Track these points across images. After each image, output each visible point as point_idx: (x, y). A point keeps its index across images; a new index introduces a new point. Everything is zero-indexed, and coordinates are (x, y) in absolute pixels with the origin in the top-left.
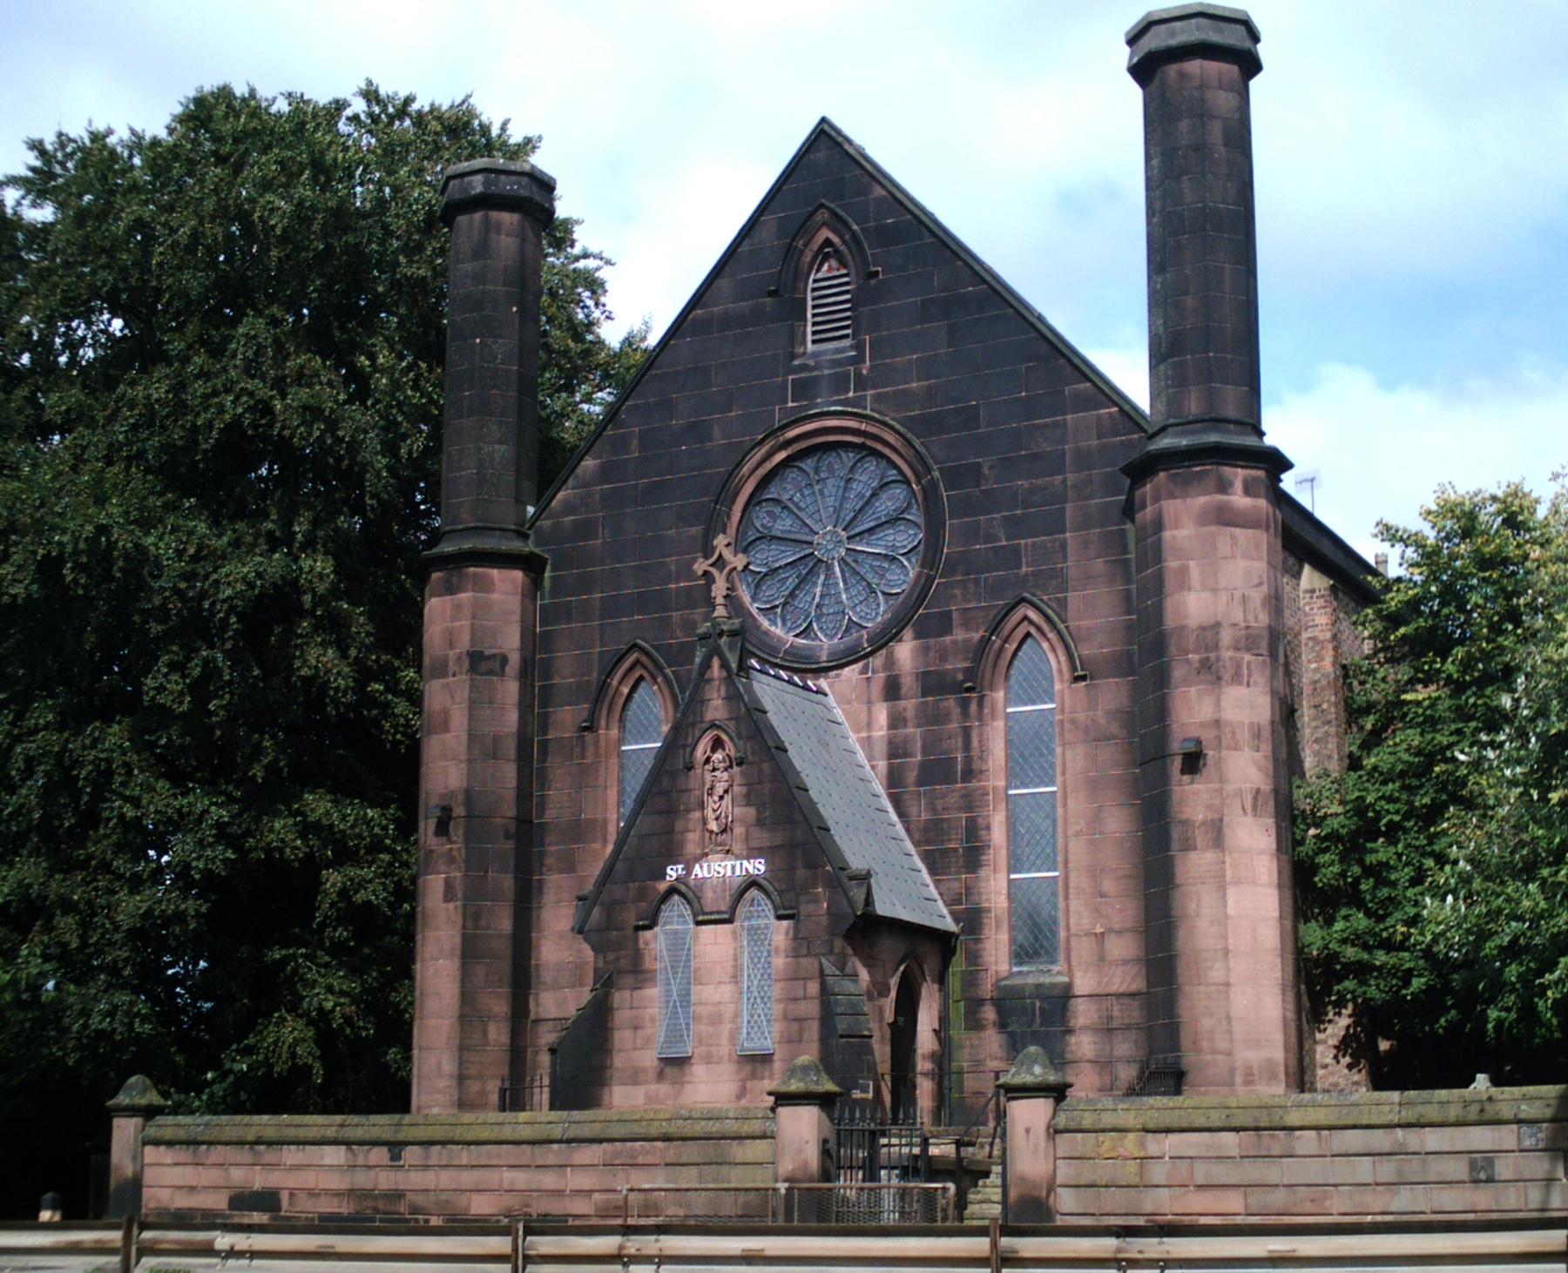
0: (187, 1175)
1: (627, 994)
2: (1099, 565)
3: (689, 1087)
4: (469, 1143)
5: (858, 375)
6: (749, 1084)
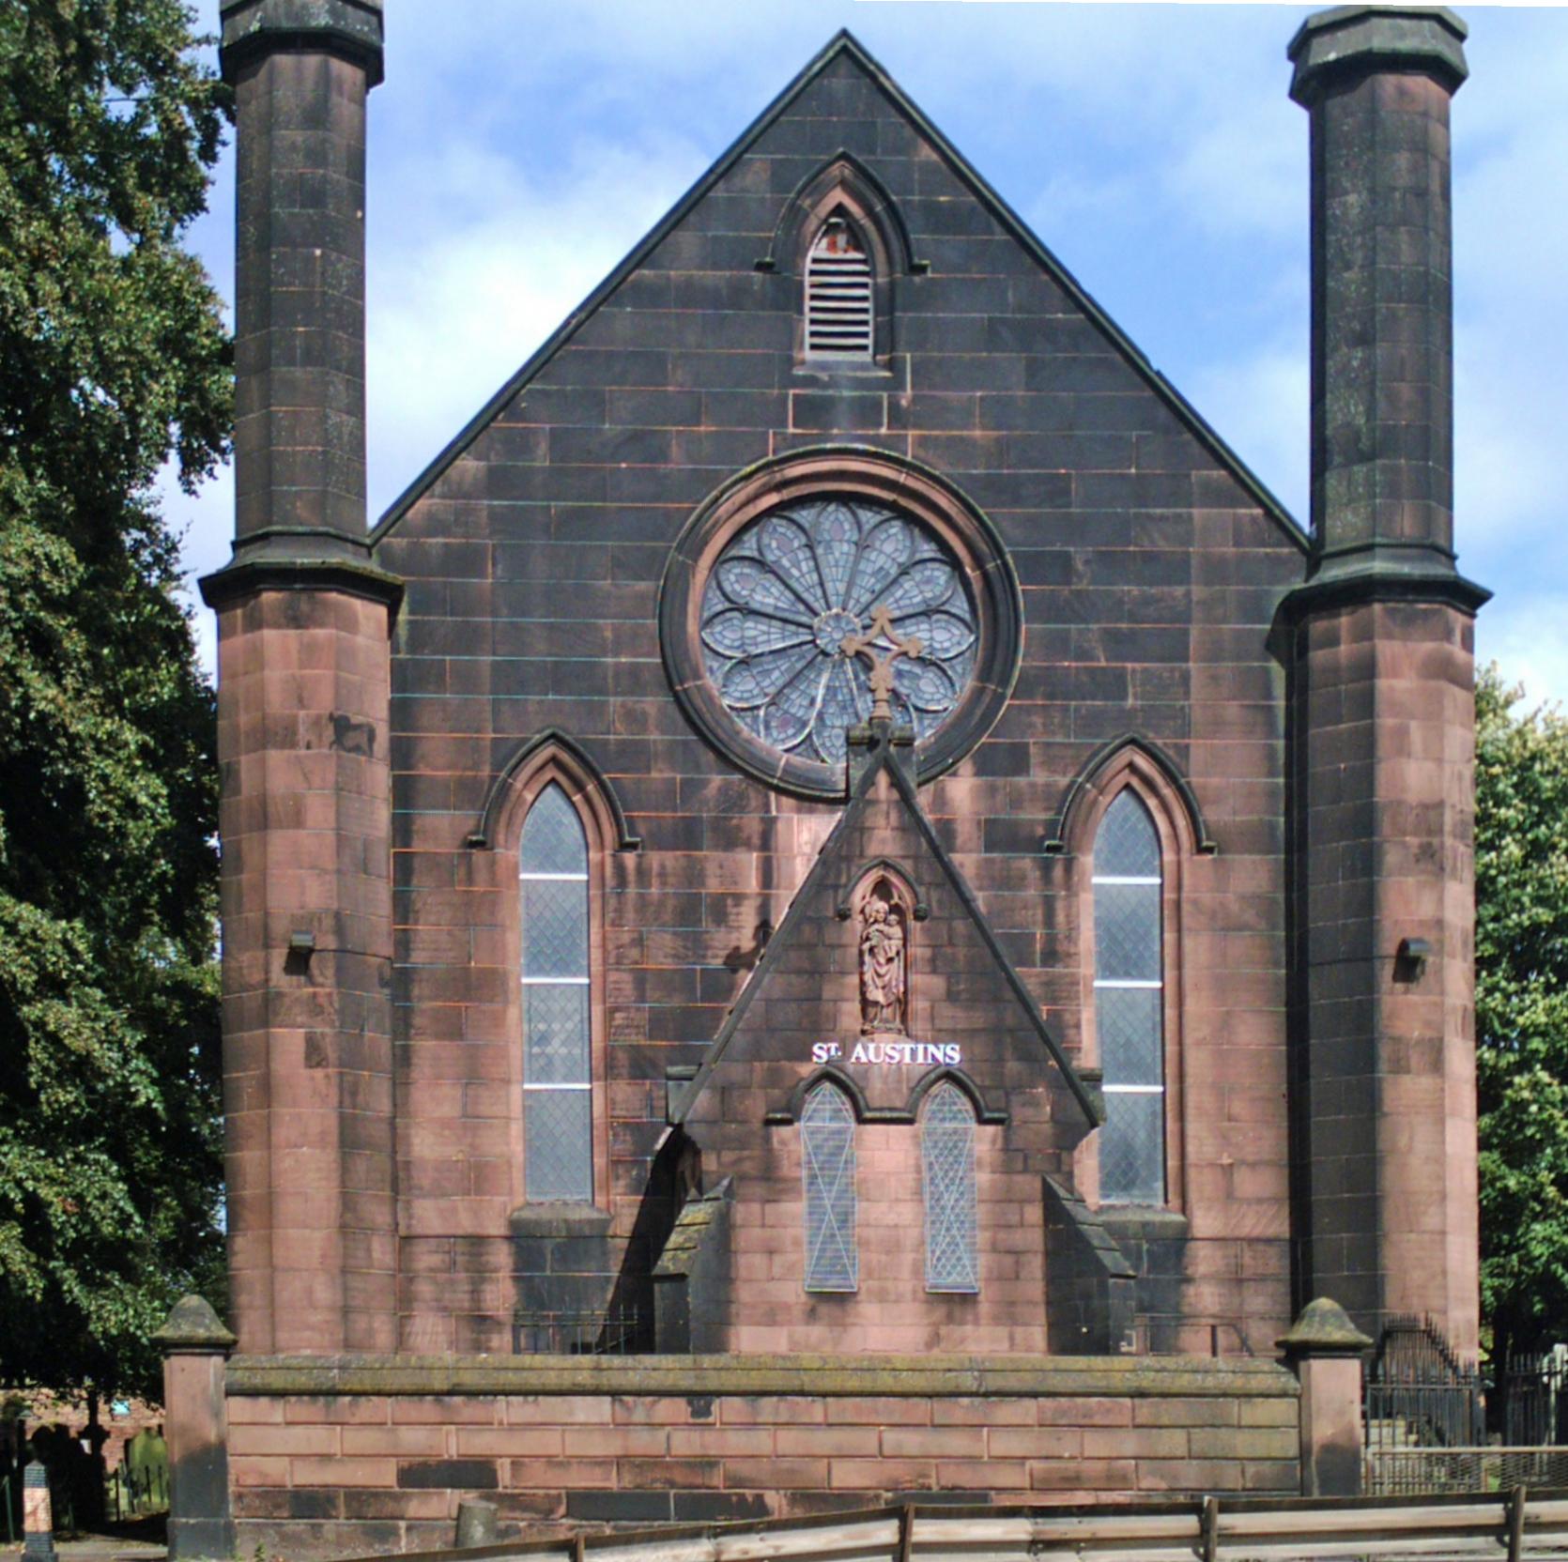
0: (319, 1439)
1: (756, 1207)
2: (1232, 710)
3: (855, 1331)
4: (824, 1395)
5: (894, 406)
6: (943, 1330)
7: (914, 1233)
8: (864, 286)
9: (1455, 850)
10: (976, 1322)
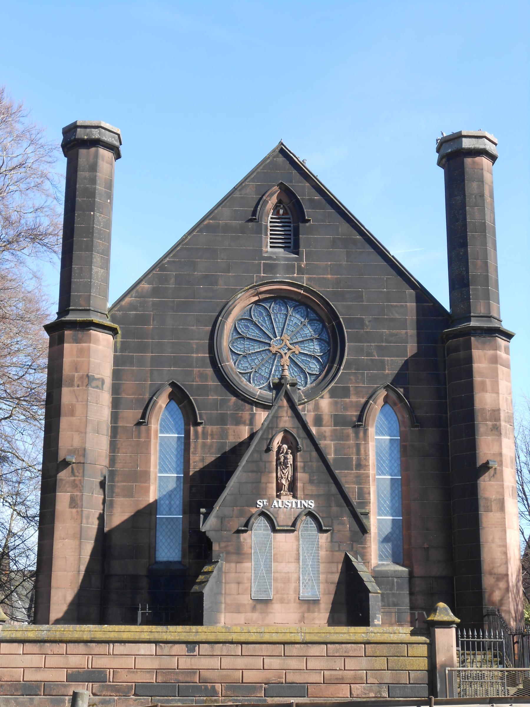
0: (37, 661)
1: (233, 565)
3: (271, 615)
5: (299, 267)
7: (295, 576)
8: (290, 226)
9: (506, 427)
10: (319, 612)
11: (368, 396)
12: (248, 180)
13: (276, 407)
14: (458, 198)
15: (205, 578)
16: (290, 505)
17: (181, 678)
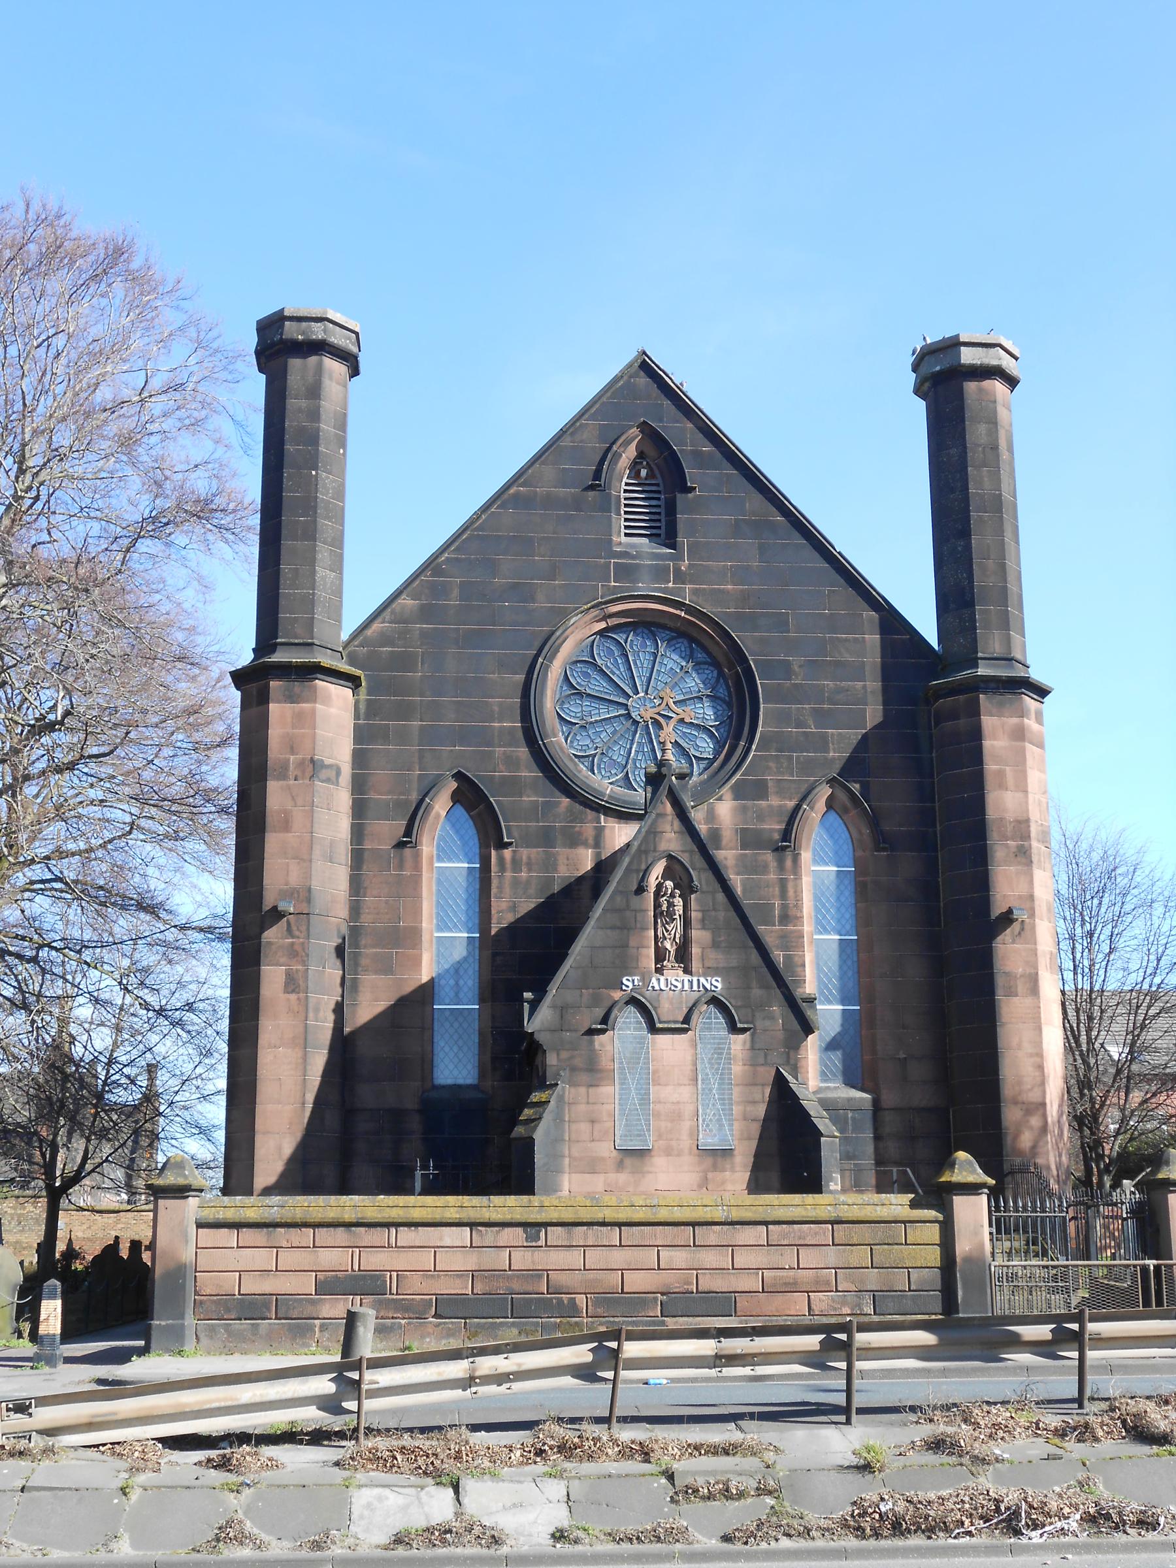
0: (263, 1258)
1: (582, 1090)
5: (677, 571)
6: (710, 1175)
8: (659, 499)
10: (733, 1170)
11: (799, 796)
12: (586, 416)
13: (653, 816)
14: (953, 451)
15: (535, 1113)
16: (679, 985)
17: (516, 1286)
